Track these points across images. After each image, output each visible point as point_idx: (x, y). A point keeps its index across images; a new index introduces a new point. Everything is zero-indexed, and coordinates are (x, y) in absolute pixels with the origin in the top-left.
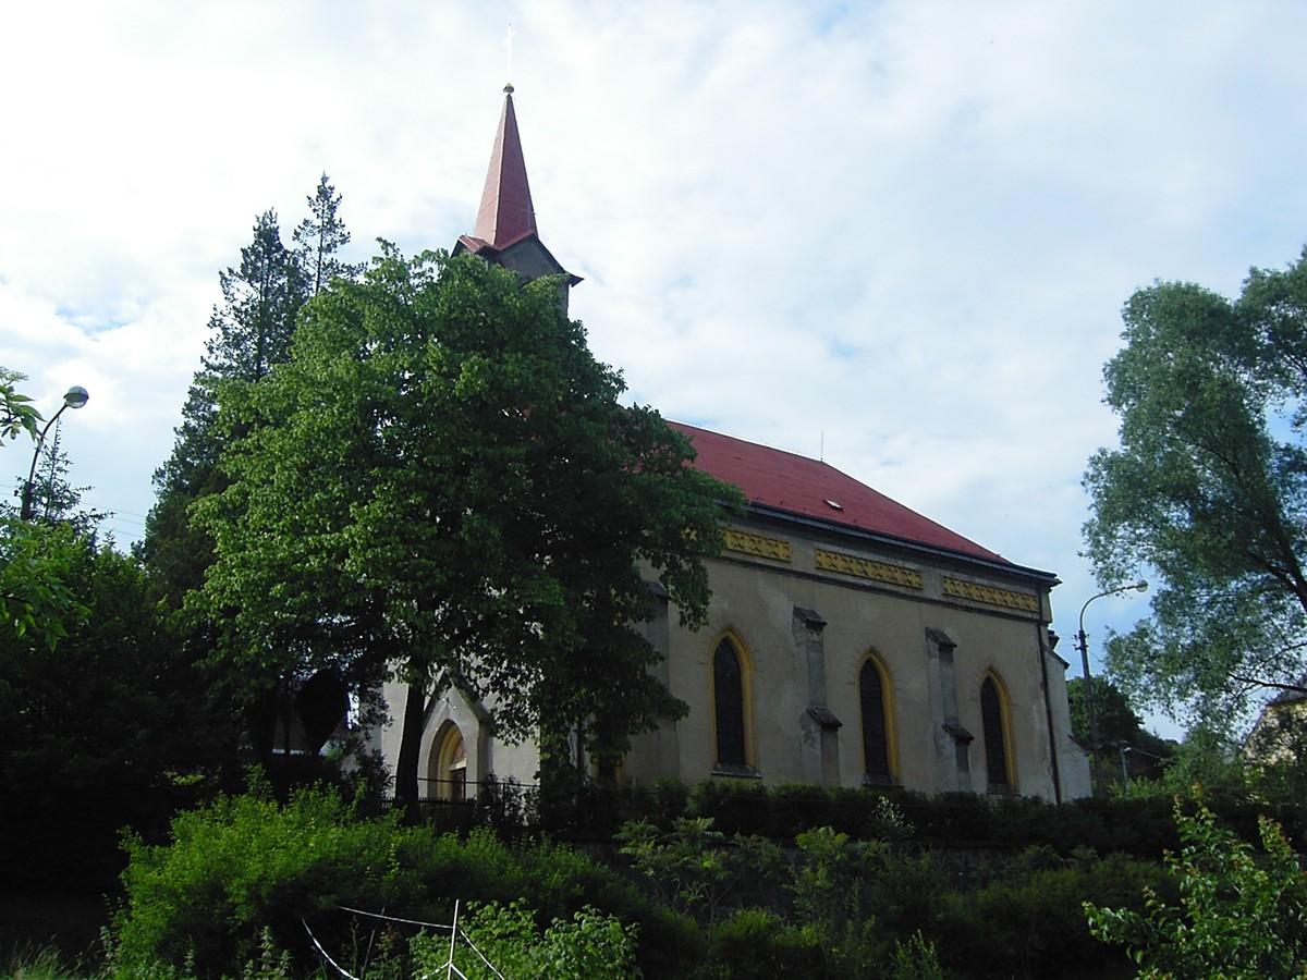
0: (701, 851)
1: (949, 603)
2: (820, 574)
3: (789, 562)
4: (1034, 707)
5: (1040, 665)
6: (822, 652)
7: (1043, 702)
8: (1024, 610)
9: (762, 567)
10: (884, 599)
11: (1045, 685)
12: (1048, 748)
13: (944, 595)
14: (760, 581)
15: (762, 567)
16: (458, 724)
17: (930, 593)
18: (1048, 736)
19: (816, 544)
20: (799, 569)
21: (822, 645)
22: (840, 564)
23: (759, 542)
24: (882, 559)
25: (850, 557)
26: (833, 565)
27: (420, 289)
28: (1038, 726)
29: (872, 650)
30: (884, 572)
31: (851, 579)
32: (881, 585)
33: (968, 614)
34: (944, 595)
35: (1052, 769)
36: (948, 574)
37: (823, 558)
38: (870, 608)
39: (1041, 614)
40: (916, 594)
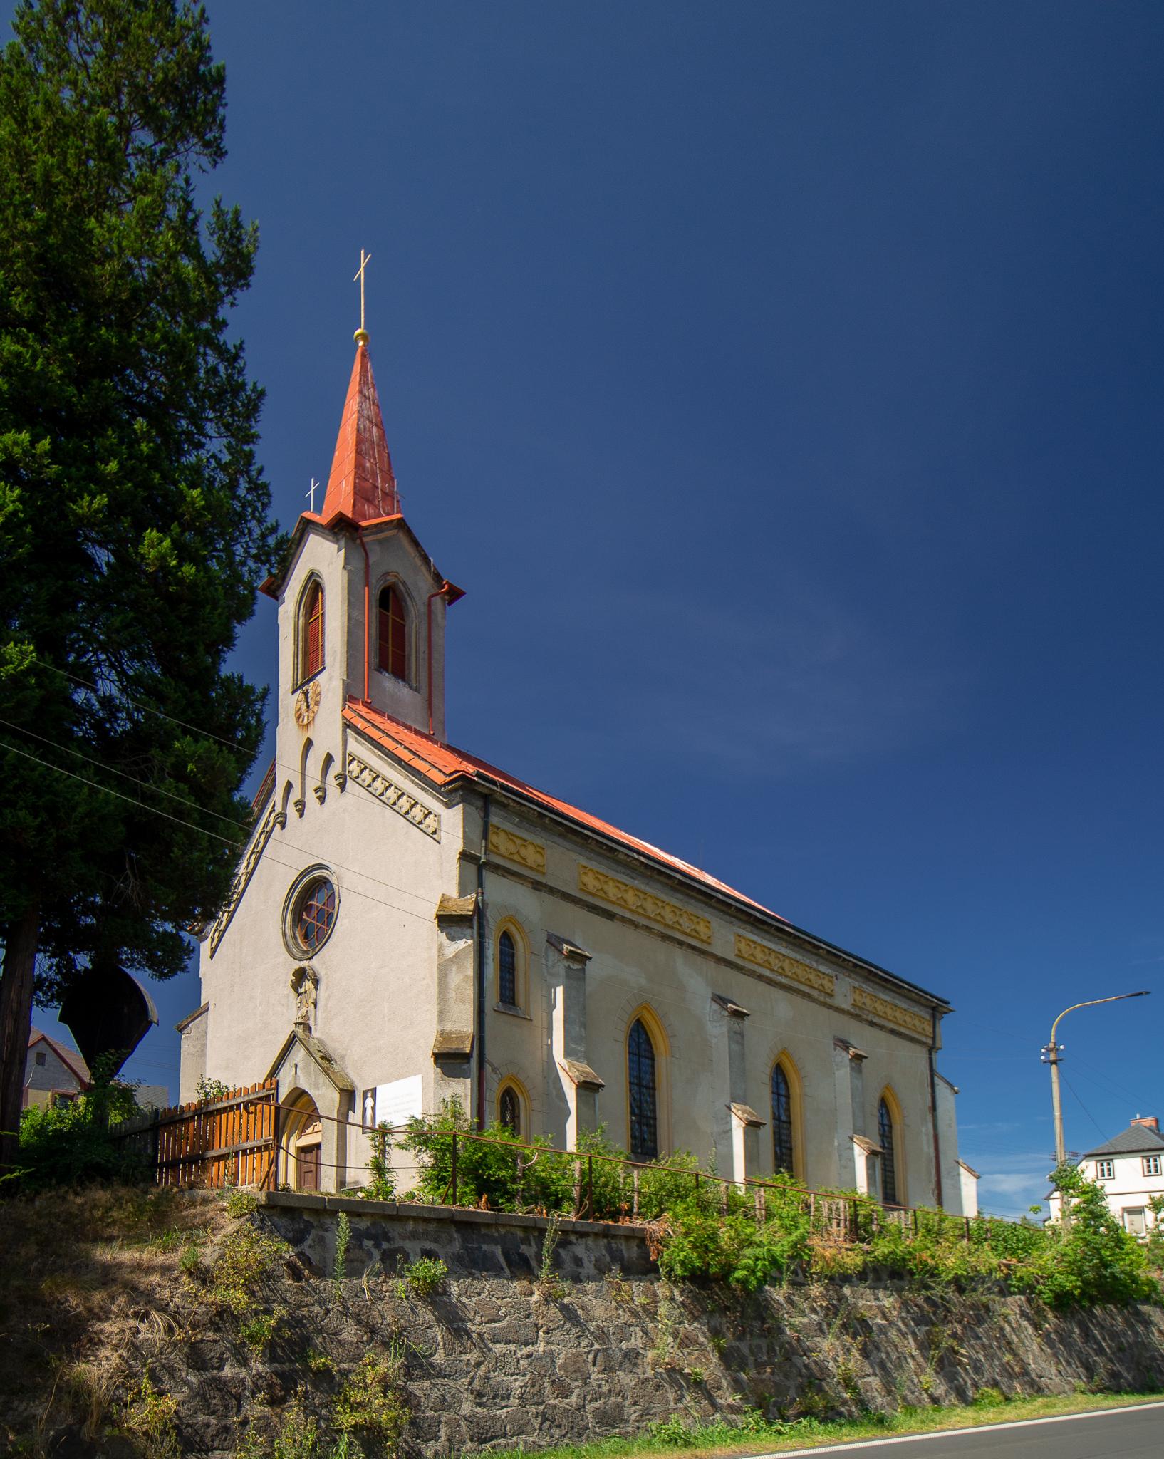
0: (197, 304)
1: (856, 1015)
2: (739, 961)
3: (709, 944)
4: (923, 1130)
5: (930, 1090)
6: (743, 1045)
7: (930, 1125)
8: (919, 1033)
9: (680, 943)
10: (798, 1000)
11: (934, 1108)
12: (933, 1171)
13: (736, 955)
14: (679, 959)
15: (680, 943)
16: (311, 1093)
17: (717, 950)
18: (934, 1160)
19: (736, 929)
20: (719, 953)
21: (743, 1037)
22: (760, 956)
23: (663, 907)
24: (799, 957)
25: (770, 949)
26: (752, 955)
27: (217, 445)
28: (925, 1148)
29: (784, 1052)
30: (799, 971)
31: (768, 973)
32: (796, 985)
33: (870, 1028)
34: (736, 955)
35: (936, 1192)
36: (857, 984)
37: (742, 945)
38: (783, 1007)
39: (934, 1038)
40: (828, 1000)
